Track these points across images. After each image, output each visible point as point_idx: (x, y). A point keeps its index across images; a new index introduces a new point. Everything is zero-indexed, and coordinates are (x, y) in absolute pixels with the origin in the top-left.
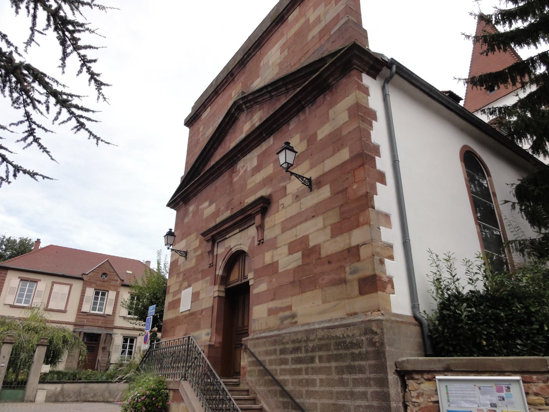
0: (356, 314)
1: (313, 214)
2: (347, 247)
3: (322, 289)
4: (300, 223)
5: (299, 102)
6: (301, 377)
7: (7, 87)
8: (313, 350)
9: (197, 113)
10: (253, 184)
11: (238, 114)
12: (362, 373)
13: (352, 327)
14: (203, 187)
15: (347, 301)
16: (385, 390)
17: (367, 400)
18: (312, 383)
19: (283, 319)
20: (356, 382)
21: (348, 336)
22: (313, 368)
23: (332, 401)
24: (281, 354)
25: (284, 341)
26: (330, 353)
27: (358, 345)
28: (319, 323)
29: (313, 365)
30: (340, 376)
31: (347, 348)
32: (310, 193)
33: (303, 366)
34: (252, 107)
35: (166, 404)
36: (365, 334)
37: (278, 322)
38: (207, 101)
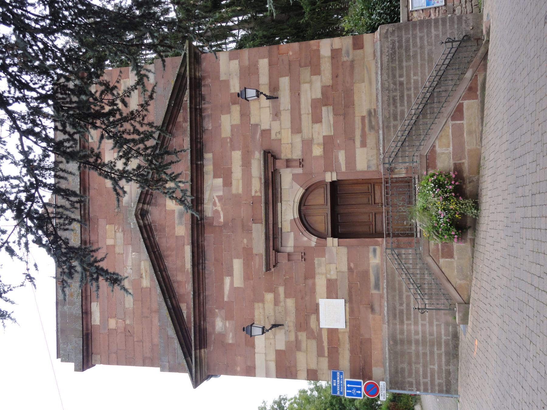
0: (374, 52)
1: (297, 94)
2: (330, 60)
3: (354, 83)
4: (300, 109)
5: (196, 109)
6: (413, 95)
7: (43, 37)
8: (395, 84)
9: (84, 332)
10: (241, 182)
11: (147, 220)
12: (409, 40)
13: (383, 49)
14: (203, 292)
15: (366, 60)
16: (418, 23)
17: (424, 36)
18: (416, 82)
19: (372, 127)
20: (415, 45)
21: (388, 51)
22: (407, 83)
23: (426, 64)
24: (397, 120)
25: (388, 117)
26: (397, 67)
27: (393, 43)
28: (377, 84)
29: (405, 83)
30: (412, 58)
31: (395, 53)
32: (279, 99)
33: (406, 93)
34: (153, 196)
35: (455, 232)
36: (387, 38)
37: (373, 132)
38: (84, 303)
